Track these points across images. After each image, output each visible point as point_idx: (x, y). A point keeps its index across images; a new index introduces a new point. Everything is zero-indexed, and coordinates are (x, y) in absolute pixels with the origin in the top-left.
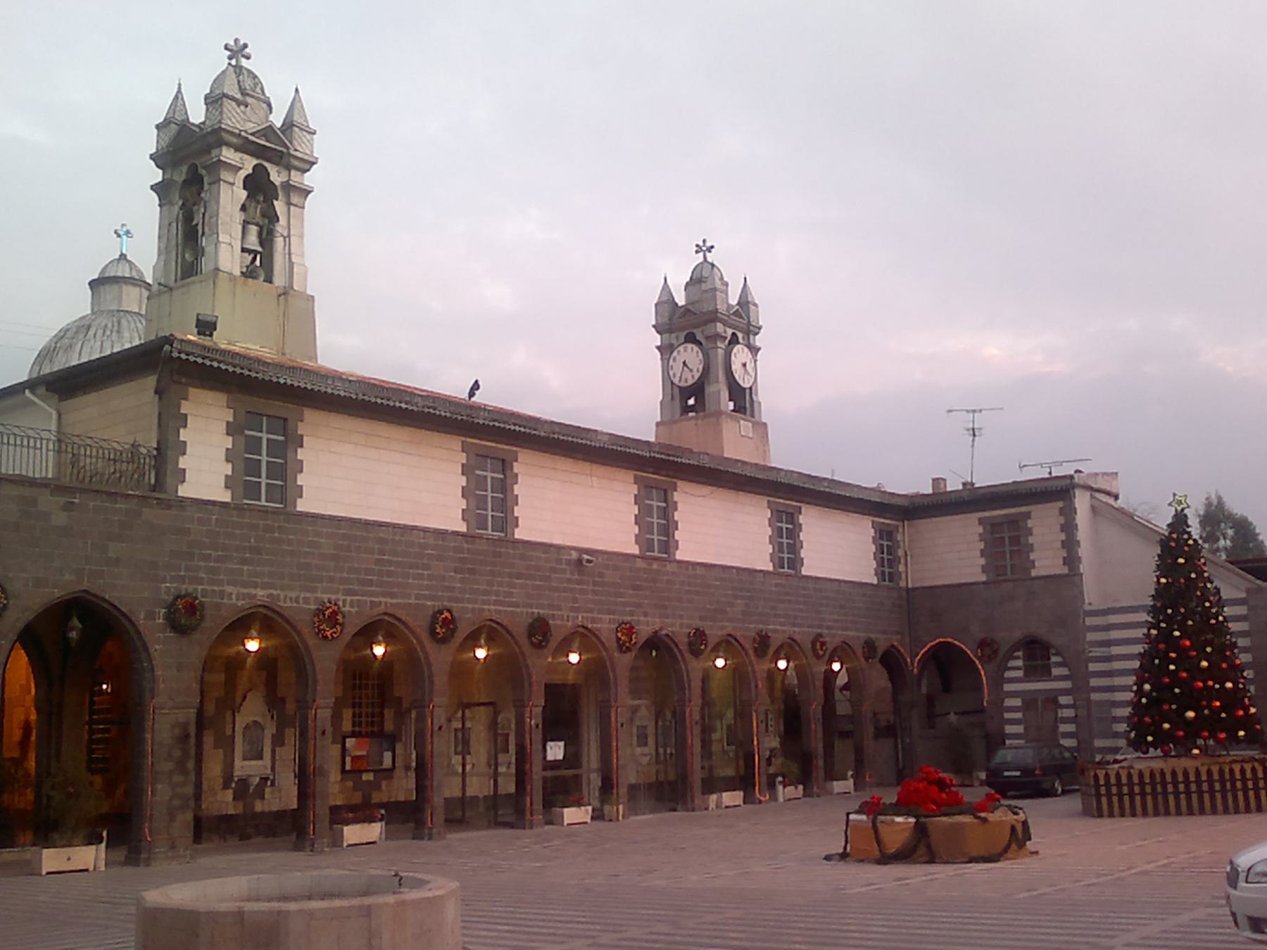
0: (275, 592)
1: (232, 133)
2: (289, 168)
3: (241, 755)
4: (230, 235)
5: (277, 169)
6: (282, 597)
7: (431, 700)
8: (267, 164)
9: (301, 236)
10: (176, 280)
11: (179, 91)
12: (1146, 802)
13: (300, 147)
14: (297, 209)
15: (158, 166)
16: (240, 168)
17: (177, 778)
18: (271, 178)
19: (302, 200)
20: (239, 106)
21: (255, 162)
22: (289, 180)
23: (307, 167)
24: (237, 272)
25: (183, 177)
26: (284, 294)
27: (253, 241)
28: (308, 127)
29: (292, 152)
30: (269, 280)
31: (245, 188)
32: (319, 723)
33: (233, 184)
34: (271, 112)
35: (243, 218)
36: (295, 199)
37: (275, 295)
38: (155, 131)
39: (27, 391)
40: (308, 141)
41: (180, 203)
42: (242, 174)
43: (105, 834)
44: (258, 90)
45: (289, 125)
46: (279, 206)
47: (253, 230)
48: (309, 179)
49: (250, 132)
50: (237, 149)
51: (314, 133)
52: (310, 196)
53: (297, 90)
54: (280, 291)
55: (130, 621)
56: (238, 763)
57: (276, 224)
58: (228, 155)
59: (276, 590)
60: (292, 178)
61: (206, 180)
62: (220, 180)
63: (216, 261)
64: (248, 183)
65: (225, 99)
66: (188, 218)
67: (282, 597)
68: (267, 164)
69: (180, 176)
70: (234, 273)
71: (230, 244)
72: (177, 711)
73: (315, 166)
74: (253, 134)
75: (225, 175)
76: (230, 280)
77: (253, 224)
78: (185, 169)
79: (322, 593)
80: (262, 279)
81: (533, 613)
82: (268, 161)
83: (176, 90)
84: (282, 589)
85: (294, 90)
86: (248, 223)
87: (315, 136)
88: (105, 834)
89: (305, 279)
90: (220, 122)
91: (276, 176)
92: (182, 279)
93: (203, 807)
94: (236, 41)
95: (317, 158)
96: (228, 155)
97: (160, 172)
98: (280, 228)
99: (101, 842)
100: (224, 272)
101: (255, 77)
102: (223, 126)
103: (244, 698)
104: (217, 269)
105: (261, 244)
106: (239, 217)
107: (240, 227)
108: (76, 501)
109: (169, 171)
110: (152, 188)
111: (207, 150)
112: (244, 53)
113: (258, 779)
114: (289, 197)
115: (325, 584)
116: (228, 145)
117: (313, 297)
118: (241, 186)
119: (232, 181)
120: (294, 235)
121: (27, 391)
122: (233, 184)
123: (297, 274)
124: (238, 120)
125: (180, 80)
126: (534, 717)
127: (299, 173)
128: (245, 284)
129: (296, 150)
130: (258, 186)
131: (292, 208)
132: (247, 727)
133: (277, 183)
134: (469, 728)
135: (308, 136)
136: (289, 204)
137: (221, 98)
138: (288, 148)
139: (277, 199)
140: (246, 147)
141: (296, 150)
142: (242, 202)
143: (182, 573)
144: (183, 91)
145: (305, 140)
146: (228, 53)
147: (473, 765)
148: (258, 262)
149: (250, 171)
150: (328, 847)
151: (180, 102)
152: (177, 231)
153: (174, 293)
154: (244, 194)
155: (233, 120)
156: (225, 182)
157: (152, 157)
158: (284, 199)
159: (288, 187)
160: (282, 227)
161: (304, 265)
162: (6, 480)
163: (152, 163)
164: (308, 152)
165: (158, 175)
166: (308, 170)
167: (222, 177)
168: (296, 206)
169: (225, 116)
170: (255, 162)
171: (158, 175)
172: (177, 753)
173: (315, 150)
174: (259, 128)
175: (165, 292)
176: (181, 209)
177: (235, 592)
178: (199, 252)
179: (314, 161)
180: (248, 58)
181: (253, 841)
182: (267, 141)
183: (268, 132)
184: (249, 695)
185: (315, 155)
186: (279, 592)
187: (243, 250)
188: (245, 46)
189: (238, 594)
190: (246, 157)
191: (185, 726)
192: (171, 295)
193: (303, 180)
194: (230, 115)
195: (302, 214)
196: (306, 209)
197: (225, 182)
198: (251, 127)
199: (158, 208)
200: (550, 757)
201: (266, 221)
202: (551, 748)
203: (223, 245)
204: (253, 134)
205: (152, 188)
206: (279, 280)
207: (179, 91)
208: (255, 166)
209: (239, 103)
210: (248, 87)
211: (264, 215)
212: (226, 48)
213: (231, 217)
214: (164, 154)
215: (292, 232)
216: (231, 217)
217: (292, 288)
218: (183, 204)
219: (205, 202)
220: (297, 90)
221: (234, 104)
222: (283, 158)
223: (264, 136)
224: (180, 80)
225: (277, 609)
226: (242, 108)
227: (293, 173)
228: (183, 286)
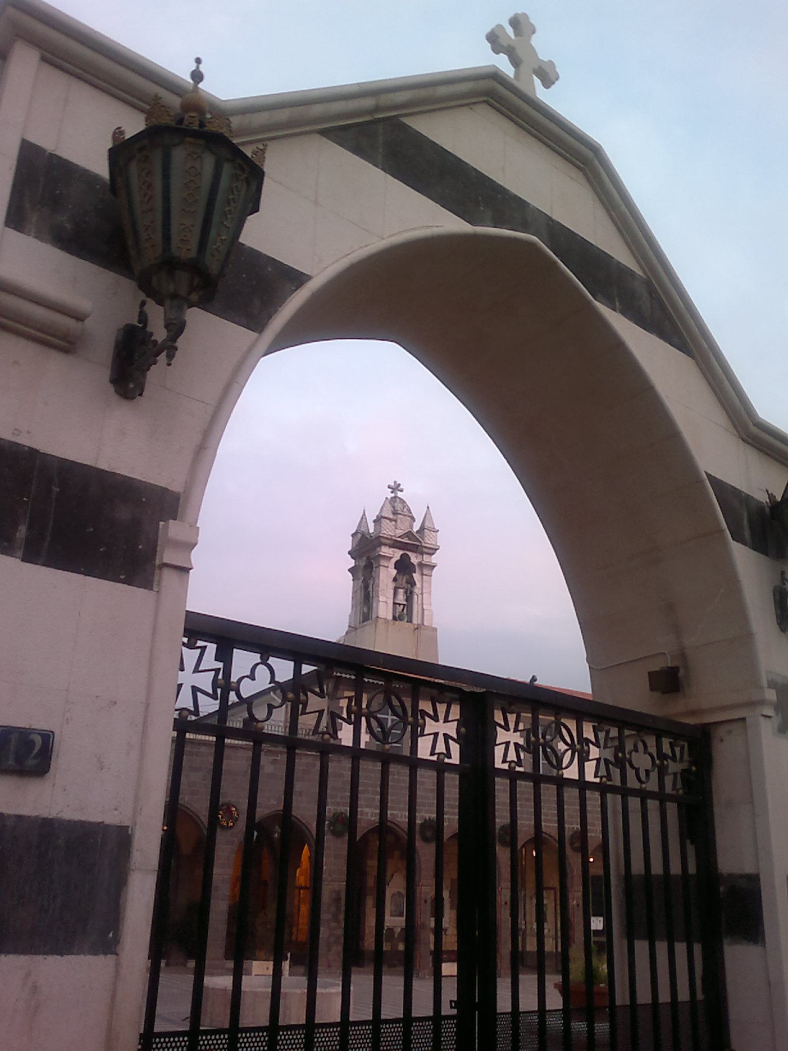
0: (395, 812)
1: (387, 538)
2: (422, 553)
3: (389, 914)
4: (386, 596)
5: (415, 554)
6: (399, 815)
7: (500, 885)
8: (410, 554)
9: (430, 593)
10: (360, 623)
11: (364, 514)
12: (522, 946)
13: (428, 541)
14: (427, 577)
15: (352, 558)
16: (391, 558)
17: (333, 924)
18: (412, 561)
19: (430, 572)
20: (391, 522)
21: (401, 552)
22: (423, 560)
23: (431, 551)
24: (390, 617)
25: (364, 563)
26: (417, 628)
27: (401, 598)
28: (434, 528)
29: (423, 544)
30: (410, 621)
31: (395, 568)
32: (423, 895)
33: (387, 567)
34: (414, 521)
35: (394, 586)
36: (425, 572)
37: (413, 628)
38: (351, 538)
39: (272, 693)
40: (433, 536)
41: (363, 578)
42: (394, 560)
43: (289, 955)
44: (405, 510)
45: (422, 528)
46: (416, 576)
47: (401, 591)
48: (434, 559)
49: (398, 536)
50: (391, 546)
51: (438, 531)
52: (435, 569)
53: (428, 507)
54: (416, 626)
55: (394, 823)
56: (387, 917)
57: (415, 587)
58: (385, 551)
59: (396, 810)
60: (424, 559)
61: (374, 566)
62: (380, 565)
63: (377, 613)
64: (397, 565)
65: (383, 520)
66: (366, 587)
67: (399, 815)
68: (410, 554)
69: (362, 563)
70: (388, 618)
71: (386, 602)
72: (333, 883)
73: (438, 551)
74: (399, 537)
75: (383, 562)
76: (385, 622)
77: (401, 588)
78: (365, 558)
79: (425, 813)
80: (406, 620)
81: (573, 828)
82: (408, 550)
83: (362, 514)
84: (399, 810)
85: (426, 508)
86: (398, 588)
87: (438, 533)
88: (289, 955)
89: (432, 619)
90: (380, 532)
91: (414, 559)
92: (363, 622)
93: (365, 944)
94: (395, 482)
95: (439, 546)
96: (385, 551)
97: (353, 561)
98: (417, 590)
99: (287, 960)
100: (381, 618)
101: (404, 502)
102: (381, 535)
103: (392, 876)
104: (377, 617)
105: (407, 600)
106: (392, 585)
107: (392, 592)
108: (279, 758)
109: (357, 560)
110: (349, 570)
111: (375, 549)
112: (399, 489)
113: (400, 929)
114: (422, 571)
115: (427, 808)
116: (385, 545)
117: (436, 629)
118: (393, 567)
119: (386, 565)
120: (426, 593)
121: (272, 693)
122: (387, 567)
123: (427, 616)
124: (388, 530)
125: (364, 507)
126: (575, 898)
127: (429, 556)
128: (394, 624)
129: (426, 543)
130: (404, 567)
131: (424, 577)
132: (394, 895)
133: (415, 563)
134: (546, 904)
135: (434, 534)
136: (422, 574)
137: (380, 519)
138: (420, 542)
139: (415, 572)
140: (396, 545)
141: (426, 543)
142: (393, 577)
143: (338, 800)
144: (366, 513)
145: (431, 536)
146: (390, 490)
147: (549, 930)
148: (405, 611)
149: (399, 558)
150: (428, 975)
151: (364, 520)
152: (360, 595)
153: (358, 631)
154: (395, 572)
155: (388, 530)
156: (384, 566)
157: (349, 553)
158: (420, 572)
159: (421, 565)
160: (419, 589)
161: (431, 610)
162: (241, 748)
163: (349, 556)
164: (433, 543)
165: (352, 563)
166: (433, 554)
167: (382, 564)
168: (426, 575)
169: (382, 529)
170: (401, 552)
171: (352, 563)
172: (333, 909)
173: (438, 541)
174: (405, 532)
175: (353, 631)
176: (363, 582)
177: (370, 812)
178: (370, 608)
179: (437, 547)
180: (401, 491)
181: (396, 968)
182: (410, 540)
183: (409, 535)
184: (395, 875)
185: (438, 544)
186: (397, 812)
187: (395, 604)
188: (399, 485)
189: (372, 813)
190: (396, 550)
191: (339, 893)
192: (356, 633)
193: (431, 559)
194: (385, 528)
195: (431, 580)
196: (432, 577)
197: (384, 566)
198: (399, 532)
199: (352, 582)
200: (593, 927)
201: (409, 586)
202: (593, 921)
203: (381, 603)
204: (399, 537)
205: (349, 570)
206: (416, 620)
207: (364, 514)
208: (402, 556)
209: (391, 520)
210: (399, 509)
211: (407, 582)
212: (389, 487)
213: (387, 586)
214: (354, 551)
215: (424, 591)
216: (387, 586)
217: (423, 624)
218: (364, 579)
219: (374, 578)
220: (428, 507)
221: (388, 521)
222: (417, 548)
223: (407, 537)
224: (364, 507)
225: (396, 822)
226: (393, 523)
227: (425, 556)
228: (362, 626)
